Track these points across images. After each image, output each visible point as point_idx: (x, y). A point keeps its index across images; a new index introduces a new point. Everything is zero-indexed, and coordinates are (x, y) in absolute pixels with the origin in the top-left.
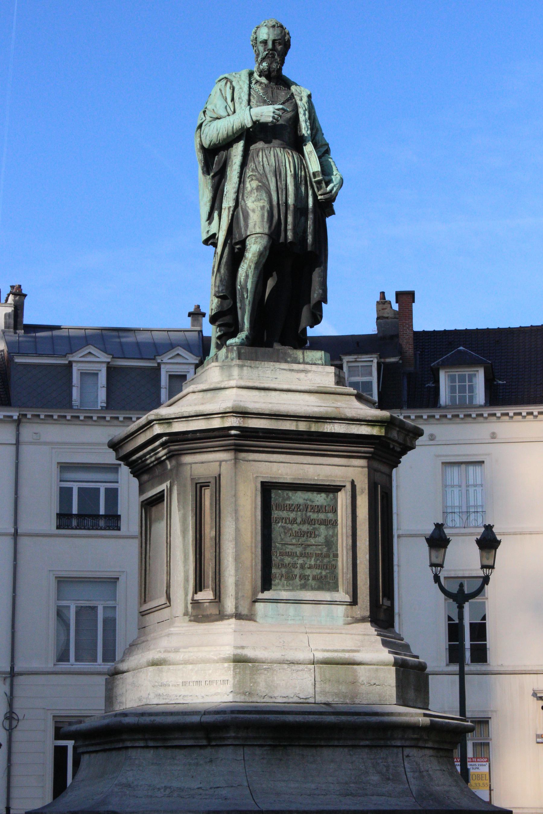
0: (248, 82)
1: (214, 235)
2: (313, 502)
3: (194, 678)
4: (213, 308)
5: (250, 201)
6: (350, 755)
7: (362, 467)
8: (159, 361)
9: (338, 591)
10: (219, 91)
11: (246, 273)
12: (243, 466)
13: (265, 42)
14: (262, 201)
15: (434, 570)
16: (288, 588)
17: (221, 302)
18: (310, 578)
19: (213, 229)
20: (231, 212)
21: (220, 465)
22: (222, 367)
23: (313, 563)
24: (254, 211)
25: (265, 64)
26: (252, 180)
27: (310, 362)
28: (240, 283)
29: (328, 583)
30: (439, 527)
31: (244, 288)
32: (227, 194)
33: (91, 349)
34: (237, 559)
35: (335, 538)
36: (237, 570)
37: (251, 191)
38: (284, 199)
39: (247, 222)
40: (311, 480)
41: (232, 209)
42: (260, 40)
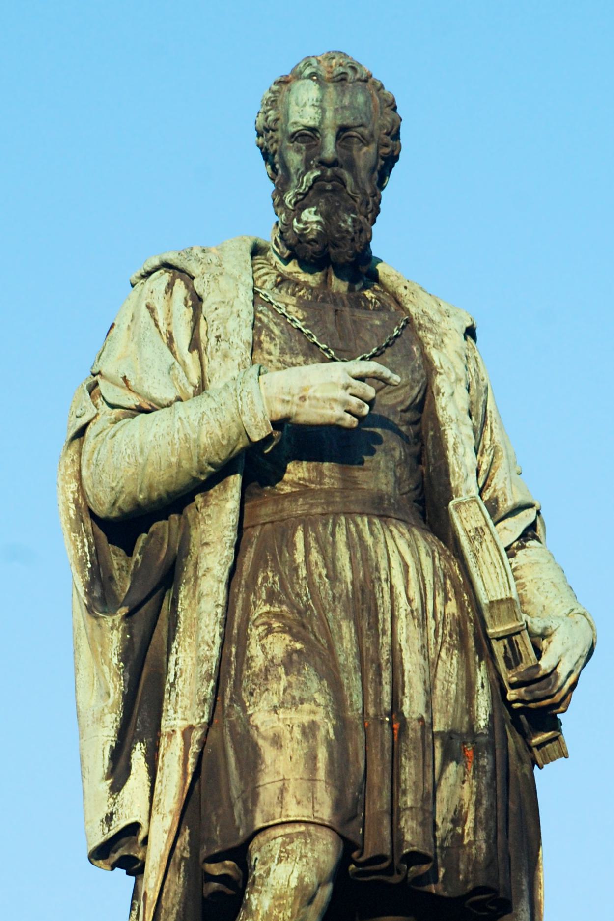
5: (263, 705)
10: (145, 312)
13: (309, 136)
14: (306, 706)
20: (194, 748)
24: (276, 741)
25: (309, 215)
26: (270, 631)
32: (180, 682)
38: (386, 698)
41: (197, 735)
42: (292, 129)
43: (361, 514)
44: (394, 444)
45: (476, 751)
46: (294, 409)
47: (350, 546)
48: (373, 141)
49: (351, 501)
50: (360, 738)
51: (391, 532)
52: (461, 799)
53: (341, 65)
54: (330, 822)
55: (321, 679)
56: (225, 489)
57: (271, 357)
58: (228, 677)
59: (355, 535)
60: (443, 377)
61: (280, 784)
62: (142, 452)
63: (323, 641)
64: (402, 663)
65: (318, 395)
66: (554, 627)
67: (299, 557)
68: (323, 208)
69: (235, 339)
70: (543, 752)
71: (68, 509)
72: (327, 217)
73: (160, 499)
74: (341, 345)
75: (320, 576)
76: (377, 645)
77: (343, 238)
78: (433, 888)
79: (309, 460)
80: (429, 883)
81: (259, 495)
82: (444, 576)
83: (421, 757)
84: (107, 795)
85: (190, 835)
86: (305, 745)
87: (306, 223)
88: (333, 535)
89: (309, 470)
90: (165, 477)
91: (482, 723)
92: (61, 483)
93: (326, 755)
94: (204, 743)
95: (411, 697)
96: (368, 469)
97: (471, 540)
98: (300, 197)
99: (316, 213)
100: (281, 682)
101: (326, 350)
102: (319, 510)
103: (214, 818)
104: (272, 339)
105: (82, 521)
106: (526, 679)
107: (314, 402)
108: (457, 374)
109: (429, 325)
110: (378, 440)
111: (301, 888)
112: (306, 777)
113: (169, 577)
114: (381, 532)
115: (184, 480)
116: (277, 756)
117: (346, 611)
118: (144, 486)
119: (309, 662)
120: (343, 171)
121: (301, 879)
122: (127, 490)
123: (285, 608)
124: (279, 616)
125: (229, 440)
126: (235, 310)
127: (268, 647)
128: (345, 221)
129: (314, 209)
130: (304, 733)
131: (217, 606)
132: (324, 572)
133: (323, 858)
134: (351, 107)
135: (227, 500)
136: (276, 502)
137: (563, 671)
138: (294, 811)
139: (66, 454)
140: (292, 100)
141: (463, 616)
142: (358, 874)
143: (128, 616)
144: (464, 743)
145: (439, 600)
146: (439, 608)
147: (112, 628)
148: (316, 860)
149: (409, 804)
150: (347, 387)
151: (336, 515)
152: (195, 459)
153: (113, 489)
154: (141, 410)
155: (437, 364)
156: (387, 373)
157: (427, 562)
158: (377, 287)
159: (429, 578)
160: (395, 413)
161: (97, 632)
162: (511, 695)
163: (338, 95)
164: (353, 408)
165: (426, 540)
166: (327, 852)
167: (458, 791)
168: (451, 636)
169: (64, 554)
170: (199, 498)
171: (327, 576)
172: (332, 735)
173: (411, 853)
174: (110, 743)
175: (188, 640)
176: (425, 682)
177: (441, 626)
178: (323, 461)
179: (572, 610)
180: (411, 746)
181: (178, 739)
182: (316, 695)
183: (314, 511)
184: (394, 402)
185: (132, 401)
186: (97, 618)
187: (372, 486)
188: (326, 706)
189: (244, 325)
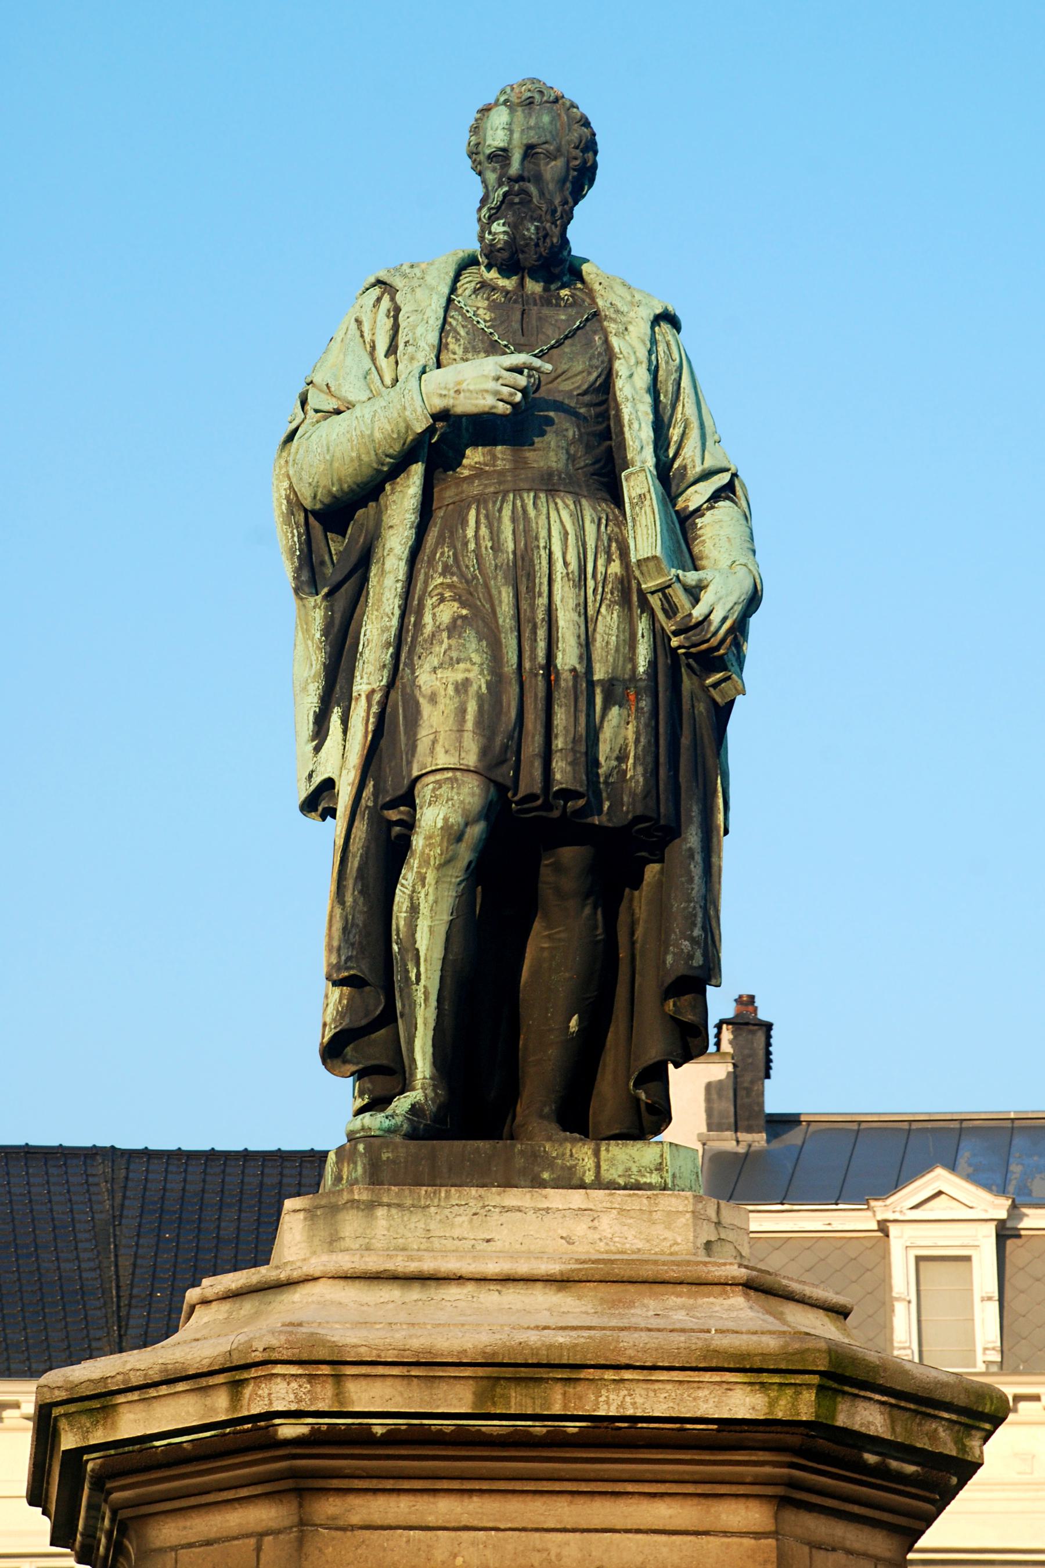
0: (446, 290)
4: (328, 1020)
5: (427, 667)
7: (757, 1535)
10: (353, 326)
11: (411, 898)
13: (501, 156)
14: (462, 666)
17: (351, 999)
20: (375, 709)
22: (310, 1213)
25: (498, 227)
26: (442, 600)
27: (621, 1181)
28: (398, 934)
31: (407, 951)
32: (367, 651)
33: (939, 1178)
37: (433, 635)
38: (541, 653)
39: (415, 734)
41: (377, 697)
42: (488, 151)
43: (529, 490)
44: (567, 425)
45: (637, 694)
46: (451, 402)
47: (514, 520)
48: (562, 155)
49: (521, 479)
50: (514, 690)
51: (556, 504)
52: (626, 739)
53: (529, 90)
54: (475, 767)
55: (480, 640)
56: (408, 477)
57: (456, 357)
58: (403, 646)
59: (520, 509)
60: (622, 361)
61: (432, 737)
62: (328, 450)
63: (487, 606)
64: (557, 621)
65: (471, 387)
66: (709, 578)
67: (470, 533)
68: (511, 219)
69: (422, 344)
70: (721, 691)
71: (281, 504)
72: (514, 227)
73: (352, 490)
74: (522, 340)
75: (486, 548)
76: (533, 607)
77: (527, 245)
78: (596, 820)
79: (484, 445)
80: (592, 815)
81: (444, 480)
82: (610, 540)
83: (573, 703)
84: (312, 755)
85: (374, 786)
86: (457, 700)
87: (495, 234)
88: (500, 510)
89: (483, 454)
90: (350, 470)
91: (641, 669)
92: (275, 483)
93: (476, 708)
94: (386, 704)
95: (564, 651)
96: (539, 450)
97: (633, 508)
98: (493, 212)
99: (504, 225)
101: (505, 346)
102: (492, 489)
103: (388, 770)
104: (457, 340)
105: (293, 514)
106: (683, 627)
107: (468, 394)
108: (637, 358)
109: (613, 316)
110: (550, 422)
111: (446, 828)
112: (455, 728)
113: (362, 563)
114: (545, 505)
115: (367, 472)
116: (432, 711)
117: (505, 578)
118: (335, 480)
119: (471, 626)
120: (528, 184)
121: (446, 820)
122: (322, 483)
123: (455, 579)
124: (451, 586)
125: (399, 434)
126: (425, 317)
128: (528, 230)
129: (502, 221)
130: (457, 690)
131: (397, 581)
132: (489, 544)
133: (469, 799)
134: (537, 127)
135: (408, 486)
136: (457, 485)
137: (716, 618)
138: (442, 760)
139: (280, 456)
140: (489, 125)
141: (628, 575)
142: (519, 811)
144: (627, 688)
145: (601, 562)
146: (601, 569)
147: (314, 607)
148: (462, 802)
149: (560, 746)
150: (497, 379)
151: (506, 493)
152: (373, 453)
153: (310, 484)
154: (338, 412)
155: (617, 350)
156: (537, 363)
157: (590, 529)
158: (579, 285)
160: (571, 397)
161: (302, 609)
162: (675, 642)
163: (525, 117)
164: (505, 397)
165: (594, 509)
166: (473, 795)
167: (623, 731)
168: (612, 593)
170: (388, 487)
171: (491, 548)
172: (484, 690)
173: (561, 790)
174: (313, 709)
175: (375, 613)
176: (579, 637)
177: (600, 585)
178: (496, 445)
179: (734, 562)
180: (562, 695)
181: (363, 699)
182: (473, 655)
183: (487, 491)
184: (572, 387)
185: (331, 404)
186: (302, 599)
187: (542, 464)
188: (482, 664)
189: (430, 329)
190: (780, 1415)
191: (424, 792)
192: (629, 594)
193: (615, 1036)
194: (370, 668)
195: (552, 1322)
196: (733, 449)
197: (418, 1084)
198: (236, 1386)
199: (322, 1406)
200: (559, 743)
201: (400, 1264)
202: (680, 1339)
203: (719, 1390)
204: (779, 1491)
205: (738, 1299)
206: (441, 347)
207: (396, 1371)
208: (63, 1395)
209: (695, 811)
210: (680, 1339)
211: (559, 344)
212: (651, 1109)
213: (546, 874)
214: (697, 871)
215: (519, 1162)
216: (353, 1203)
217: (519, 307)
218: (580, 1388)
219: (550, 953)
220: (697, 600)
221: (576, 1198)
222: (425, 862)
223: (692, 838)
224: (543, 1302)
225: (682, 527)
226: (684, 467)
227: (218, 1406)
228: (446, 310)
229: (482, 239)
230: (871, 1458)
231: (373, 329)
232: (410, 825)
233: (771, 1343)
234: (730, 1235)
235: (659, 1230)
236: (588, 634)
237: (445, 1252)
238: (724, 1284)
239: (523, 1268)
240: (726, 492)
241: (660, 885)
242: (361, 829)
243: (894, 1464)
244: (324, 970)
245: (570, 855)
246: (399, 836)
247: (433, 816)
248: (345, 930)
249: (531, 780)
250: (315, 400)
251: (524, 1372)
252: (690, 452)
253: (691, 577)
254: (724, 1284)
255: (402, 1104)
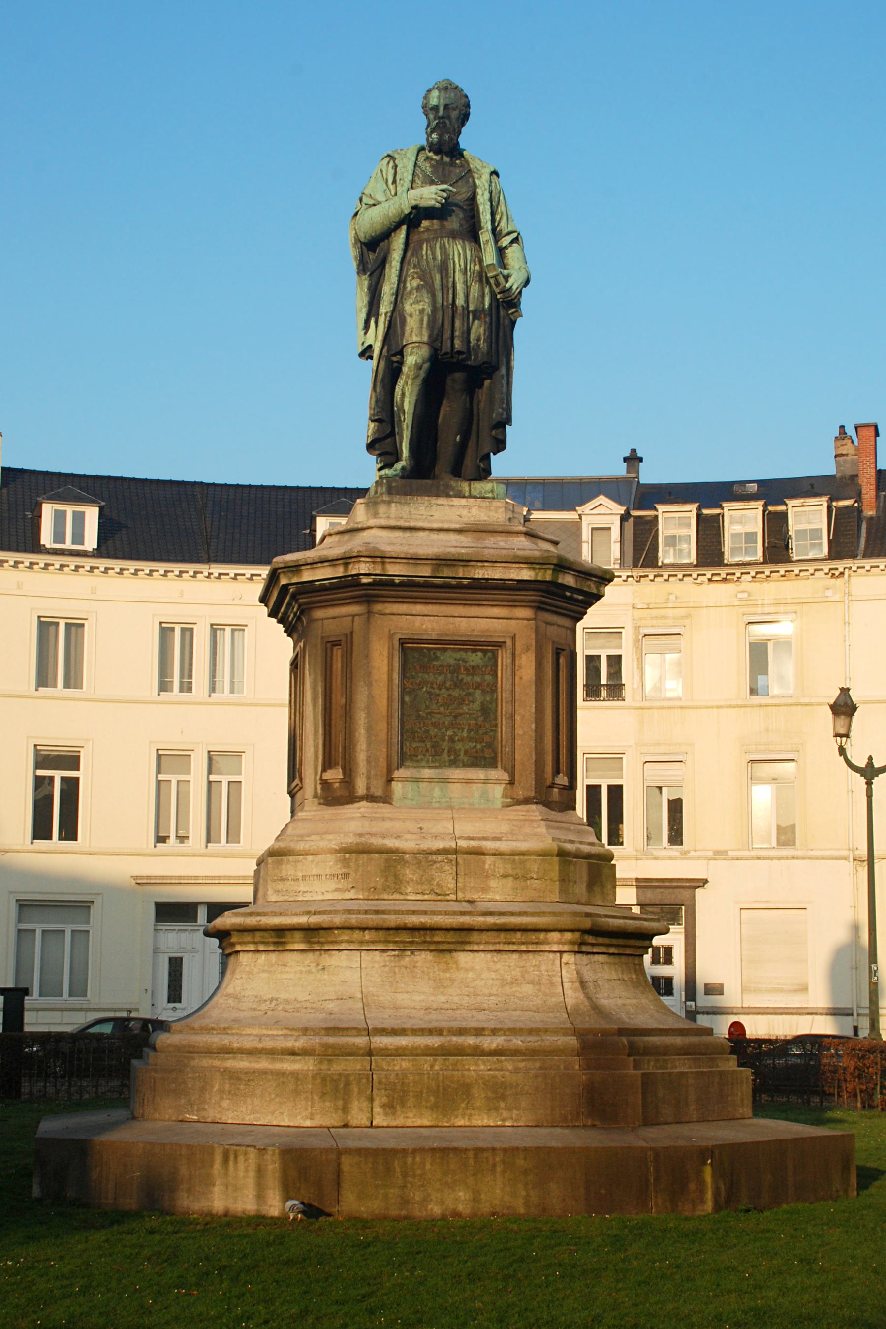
0: (414, 159)
1: (370, 346)
2: (466, 662)
3: (314, 872)
5: (408, 303)
6: (494, 962)
7: (528, 620)
8: (580, 513)
9: (497, 767)
12: (377, 620)
13: (435, 109)
15: (839, 741)
16: (434, 765)
17: (378, 427)
18: (462, 753)
19: (370, 339)
20: (388, 319)
21: (353, 621)
22: (367, 504)
23: (465, 734)
24: (411, 315)
25: (434, 136)
26: (413, 278)
29: (484, 756)
30: (845, 691)
34: (369, 729)
35: (494, 704)
36: (369, 744)
40: (462, 636)
41: (389, 314)
47: (441, 248)
58: (399, 295)
67: (424, 253)
72: (440, 136)
76: (448, 281)
78: (469, 363)
100: (415, 294)
111: (416, 364)
113: (383, 263)
115: (386, 228)
124: (416, 273)
127: (412, 283)
137: (514, 288)
138: (415, 339)
143: (370, 275)
150: (436, 194)
151: (437, 238)
154: (374, 205)
156: (451, 188)
157: (468, 253)
159: (469, 258)
162: (499, 297)
169: (350, 255)
190: (539, 579)
191: (408, 350)
192: (482, 277)
193: (472, 443)
194: (386, 303)
195: (458, 545)
196: (517, 225)
197: (404, 459)
198: (346, 565)
199: (377, 572)
200: (457, 333)
201: (402, 523)
202: (505, 552)
203: (518, 570)
204: (537, 605)
205: (522, 539)
206: (413, 181)
207: (404, 561)
208: (282, 565)
209: (504, 361)
210: (505, 552)
211: (457, 181)
212: (484, 470)
213: (449, 382)
214: (504, 382)
215: (442, 488)
216: (384, 501)
217: (441, 167)
218: (469, 568)
219: (449, 412)
220: (507, 281)
221: (463, 501)
222: (408, 377)
223: (503, 371)
224: (453, 537)
225: (501, 252)
226: (501, 230)
227: (340, 572)
228: (415, 167)
229: (428, 140)
230: (568, 594)
231: (387, 174)
232: (401, 363)
233: (537, 554)
234: (517, 516)
235: (492, 514)
236: (467, 292)
237: (417, 520)
238: (518, 533)
239: (446, 526)
240: (516, 240)
241: (490, 388)
242: (382, 364)
243: (575, 596)
244: (368, 416)
245: (458, 376)
246: (397, 367)
247: (411, 360)
248: (376, 401)
249: (447, 347)
250: (366, 200)
251: (449, 562)
252: (503, 224)
253: (505, 272)
254: (518, 533)
255: (398, 466)
